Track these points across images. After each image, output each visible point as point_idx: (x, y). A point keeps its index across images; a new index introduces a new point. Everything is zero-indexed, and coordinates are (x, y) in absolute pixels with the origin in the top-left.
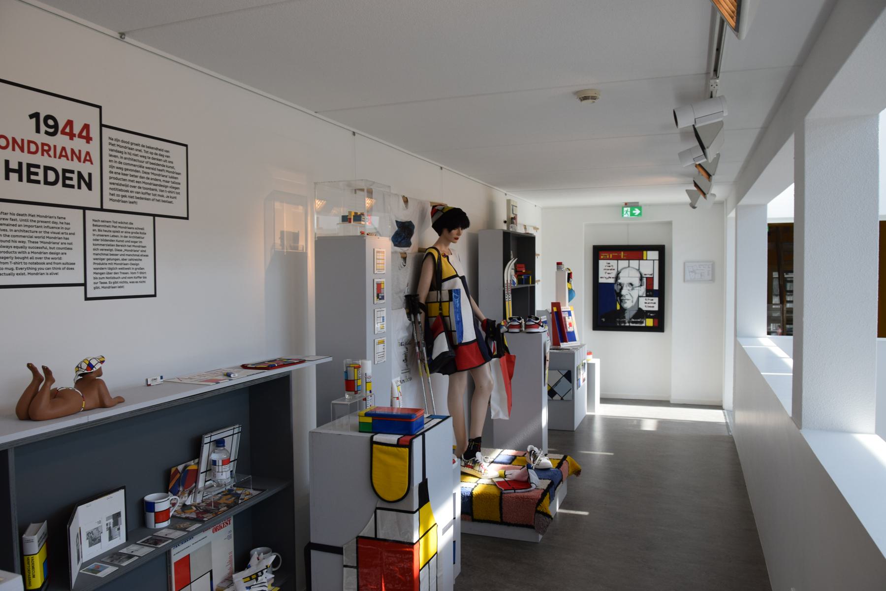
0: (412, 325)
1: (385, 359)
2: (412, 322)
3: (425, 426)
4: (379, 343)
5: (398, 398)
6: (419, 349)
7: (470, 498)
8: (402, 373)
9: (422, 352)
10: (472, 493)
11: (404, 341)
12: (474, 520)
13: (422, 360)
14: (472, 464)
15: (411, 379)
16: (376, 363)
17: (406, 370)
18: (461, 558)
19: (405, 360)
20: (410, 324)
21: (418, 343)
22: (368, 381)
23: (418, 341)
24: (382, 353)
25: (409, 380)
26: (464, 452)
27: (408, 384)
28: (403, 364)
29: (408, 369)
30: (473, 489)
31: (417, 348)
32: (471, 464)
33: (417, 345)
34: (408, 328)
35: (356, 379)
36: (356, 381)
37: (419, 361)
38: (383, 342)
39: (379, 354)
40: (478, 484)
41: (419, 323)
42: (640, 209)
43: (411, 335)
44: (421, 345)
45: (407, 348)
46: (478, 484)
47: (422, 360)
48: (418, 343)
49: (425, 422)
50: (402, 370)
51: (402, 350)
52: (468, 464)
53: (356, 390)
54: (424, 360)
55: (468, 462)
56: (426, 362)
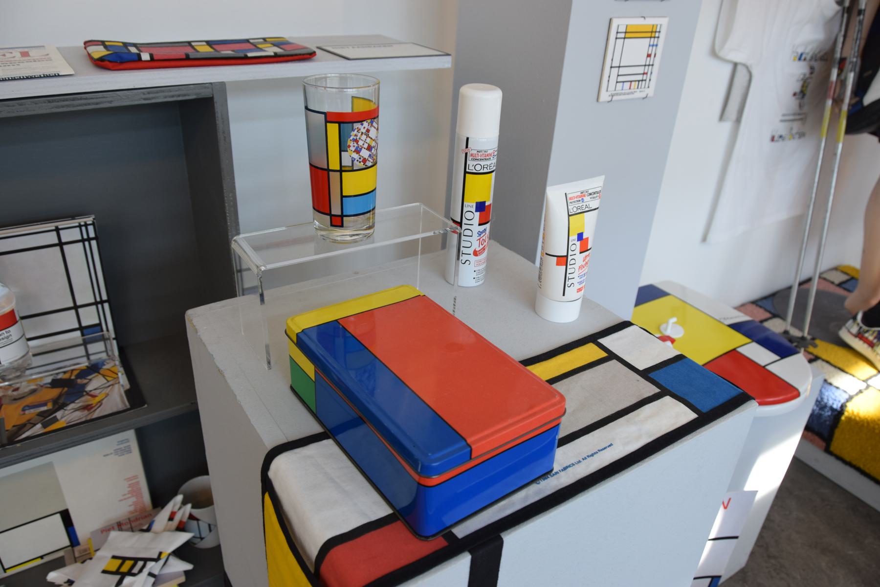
0: (840, 15)
1: (650, 92)
2: (844, 8)
3: (562, 455)
4: (629, 34)
5: (563, 260)
6: (839, 75)
7: (836, 413)
8: (782, 121)
9: (842, 83)
10: (843, 407)
11: (809, 50)
12: (828, 450)
13: (838, 101)
14: (875, 338)
15: (802, 135)
16: (605, 96)
17: (794, 114)
18: (764, 527)
19: (801, 94)
20: (837, 13)
21: (842, 61)
22: (471, 168)
23: (844, 55)
24: (641, 70)
25: (797, 136)
26: (867, 308)
27: (791, 145)
28: (792, 104)
29: (799, 114)
30: (851, 398)
31: (835, 73)
32: (871, 338)
33: (837, 66)
34: (829, 22)
35: (334, 165)
36: (334, 176)
37: (829, 102)
38: (653, 33)
39: (622, 71)
40: (865, 381)
41: (860, 12)
42: (148, 405)
43: (831, 42)
44: (848, 66)
45: (812, 69)
46: (868, 387)
47: (838, 101)
48: (842, 61)
49: (562, 433)
50: (784, 115)
51: (800, 69)
52: (866, 335)
53: (336, 210)
54: (842, 101)
55: (867, 331)
56: (845, 107)
